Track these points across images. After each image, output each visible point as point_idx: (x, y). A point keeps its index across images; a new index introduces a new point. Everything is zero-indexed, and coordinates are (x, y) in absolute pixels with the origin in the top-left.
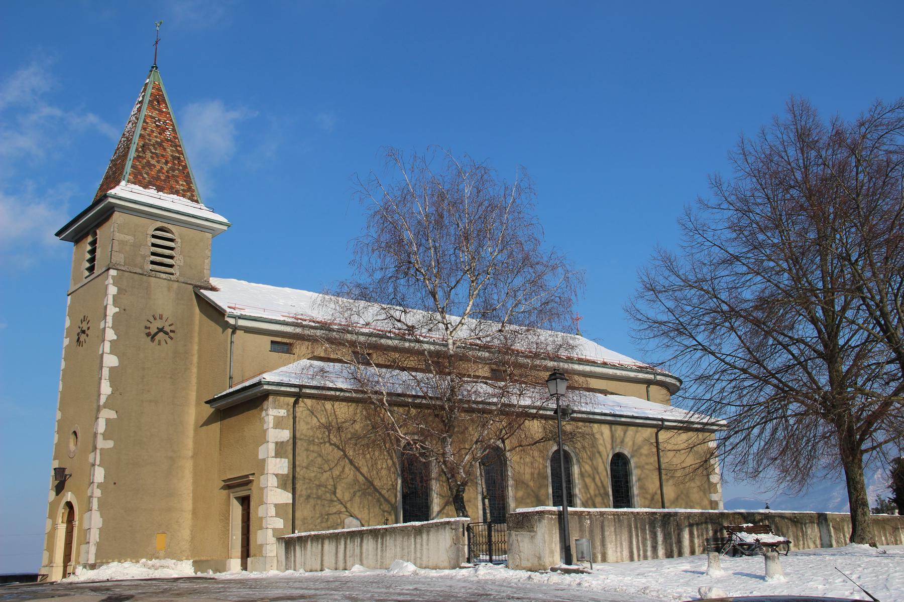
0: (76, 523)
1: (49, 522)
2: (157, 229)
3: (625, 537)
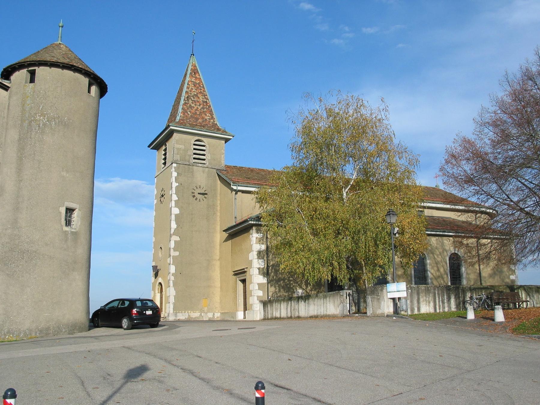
0: (164, 293)
1: (153, 292)
2: (195, 141)
3: (431, 298)
